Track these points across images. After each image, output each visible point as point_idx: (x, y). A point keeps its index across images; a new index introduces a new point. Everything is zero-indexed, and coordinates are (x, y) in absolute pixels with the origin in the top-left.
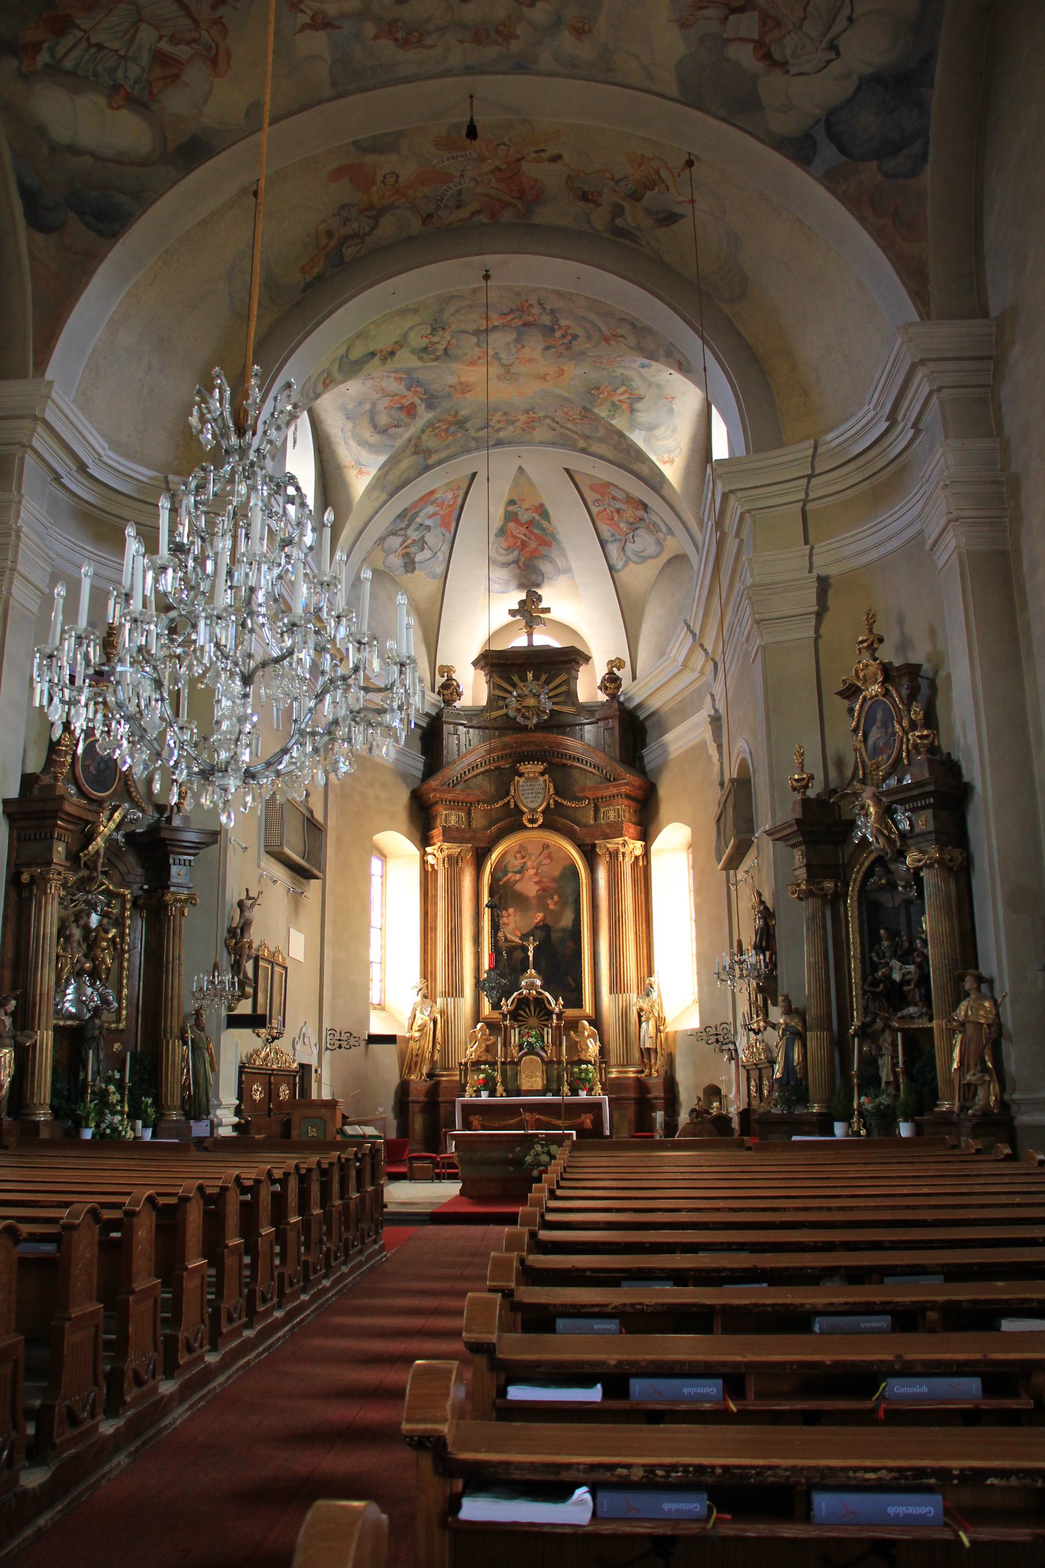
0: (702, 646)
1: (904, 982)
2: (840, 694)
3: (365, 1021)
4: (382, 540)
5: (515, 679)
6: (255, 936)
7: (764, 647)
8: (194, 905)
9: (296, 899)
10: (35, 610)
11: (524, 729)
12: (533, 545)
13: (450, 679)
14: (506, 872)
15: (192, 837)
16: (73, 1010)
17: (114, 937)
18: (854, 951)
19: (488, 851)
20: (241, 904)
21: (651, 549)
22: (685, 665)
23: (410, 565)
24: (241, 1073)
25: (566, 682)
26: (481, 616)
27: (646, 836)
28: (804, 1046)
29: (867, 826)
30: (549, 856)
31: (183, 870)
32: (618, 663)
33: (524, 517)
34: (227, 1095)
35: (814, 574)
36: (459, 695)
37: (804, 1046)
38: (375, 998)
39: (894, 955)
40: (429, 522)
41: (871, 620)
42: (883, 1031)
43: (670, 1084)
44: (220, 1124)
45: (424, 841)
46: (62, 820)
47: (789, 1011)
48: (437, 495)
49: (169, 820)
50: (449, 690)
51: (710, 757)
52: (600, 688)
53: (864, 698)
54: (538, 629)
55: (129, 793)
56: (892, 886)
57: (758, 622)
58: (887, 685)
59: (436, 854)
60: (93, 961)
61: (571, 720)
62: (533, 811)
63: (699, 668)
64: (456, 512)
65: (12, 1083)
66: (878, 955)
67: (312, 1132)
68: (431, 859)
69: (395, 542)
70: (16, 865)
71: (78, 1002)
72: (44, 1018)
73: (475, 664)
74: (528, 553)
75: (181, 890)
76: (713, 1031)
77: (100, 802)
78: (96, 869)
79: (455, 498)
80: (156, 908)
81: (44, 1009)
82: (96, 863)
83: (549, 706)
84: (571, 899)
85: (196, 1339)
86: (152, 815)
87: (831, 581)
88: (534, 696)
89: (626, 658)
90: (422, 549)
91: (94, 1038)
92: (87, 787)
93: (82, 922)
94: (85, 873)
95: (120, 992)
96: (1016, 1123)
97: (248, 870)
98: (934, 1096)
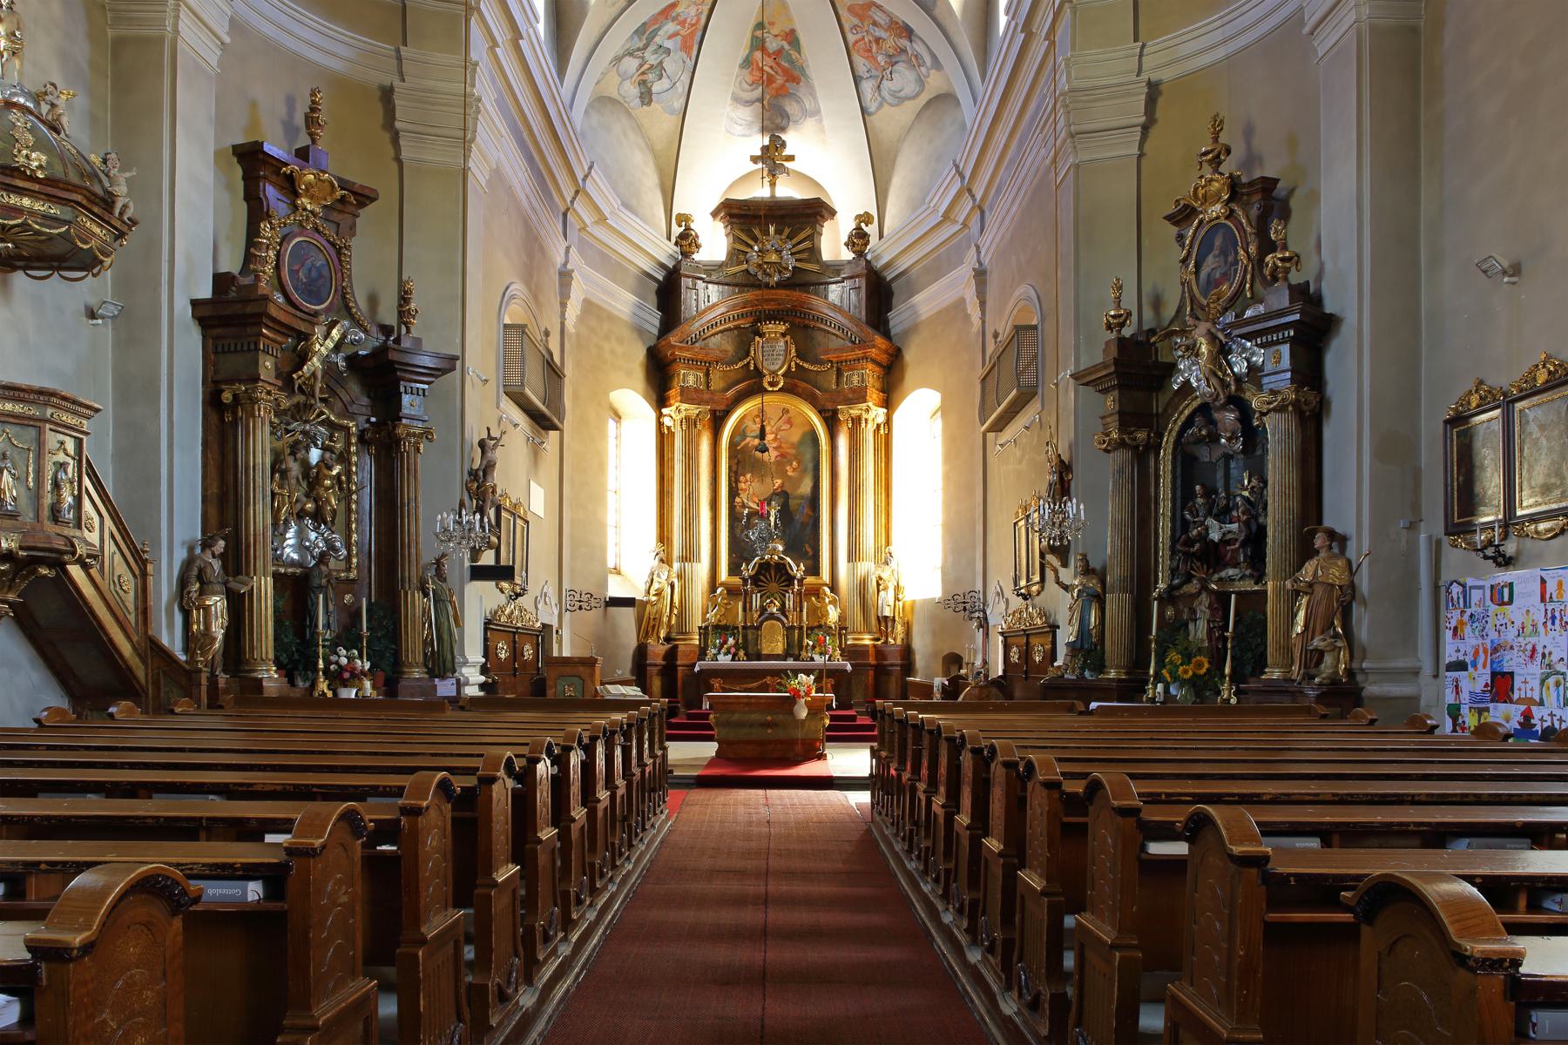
0: (970, 191)
1: (1224, 542)
2: (1169, 218)
3: (604, 584)
4: (618, 60)
5: (757, 232)
6: (498, 478)
7: (1077, 166)
8: (431, 440)
9: (536, 450)
10: (214, 63)
11: (767, 286)
12: (780, 80)
13: (688, 228)
14: (744, 436)
15: (427, 361)
16: (295, 557)
17: (339, 475)
18: (1165, 507)
19: (727, 413)
20: (482, 444)
21: (911, 88)
22: (946, 216)
23: (646, 97)
24: (486, 629)
25: (810, 238)
26: (721, 159)
27: (888, 403)
28: (1102, 610)
29: (1192, 373)
30: (789, 422)
31: (418, 400)
32: (865, 218)
33: (772, 45)
34: (473, 653)
35: (1144, 77)
36: (698, 246)
37: (1102, 610)
38: (611, 564)
39: (1209, 513)
40: (668, 44)
41: (1217, 126)
42: (1199, 593)
43: (907, 651)
44: (467, 684)
45: (660, 401)
46: (268, 327)
47: (1087, 571)
48: (679, 9)
49: (398, 341)
50: (687, 241)
51: (967, 317)
52: (847, 244)
53: (1201, 222)
54: (781, 180)
55: (348, 309)
56: (1214, 438)
57: (1072, 136)
58: (1234, 206)
59: (674, 414)
60: (316, 501)
61: (813, 278)
62: (774, 373)
63: (961, 220)
64: (699, 34)
65: (226, 636)
66: (1191, 513)
67: (570, 692)
68: (667, 421)
69: (631, 64)
70: (215, 382)
71: (300, 547)
72: (260, 563)
73: (714, 214)
74: (776, 87)
75: (415, 423)
76: (960, 599)
77: (316, 314)
78: (313, 396)
79: (698, 15)
80: (386, 443)
81: (260, 553)
82: (313, 387)
83: (791, 263)
84: (810, 466)
85: (509, 983)
86: (376, 340)
87: (1162, 87)
88: (777, 251)
89: (874, 212)
90: (661, 77)
91: (321, 587)
92: (296, 297)
93: (299, 455)
94: (301, 398)
95: (349, 537)
96: (1364, 694)
97: (485, 408)
98: (1261, 664)
